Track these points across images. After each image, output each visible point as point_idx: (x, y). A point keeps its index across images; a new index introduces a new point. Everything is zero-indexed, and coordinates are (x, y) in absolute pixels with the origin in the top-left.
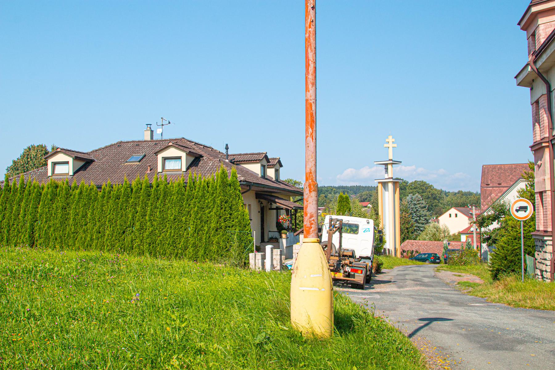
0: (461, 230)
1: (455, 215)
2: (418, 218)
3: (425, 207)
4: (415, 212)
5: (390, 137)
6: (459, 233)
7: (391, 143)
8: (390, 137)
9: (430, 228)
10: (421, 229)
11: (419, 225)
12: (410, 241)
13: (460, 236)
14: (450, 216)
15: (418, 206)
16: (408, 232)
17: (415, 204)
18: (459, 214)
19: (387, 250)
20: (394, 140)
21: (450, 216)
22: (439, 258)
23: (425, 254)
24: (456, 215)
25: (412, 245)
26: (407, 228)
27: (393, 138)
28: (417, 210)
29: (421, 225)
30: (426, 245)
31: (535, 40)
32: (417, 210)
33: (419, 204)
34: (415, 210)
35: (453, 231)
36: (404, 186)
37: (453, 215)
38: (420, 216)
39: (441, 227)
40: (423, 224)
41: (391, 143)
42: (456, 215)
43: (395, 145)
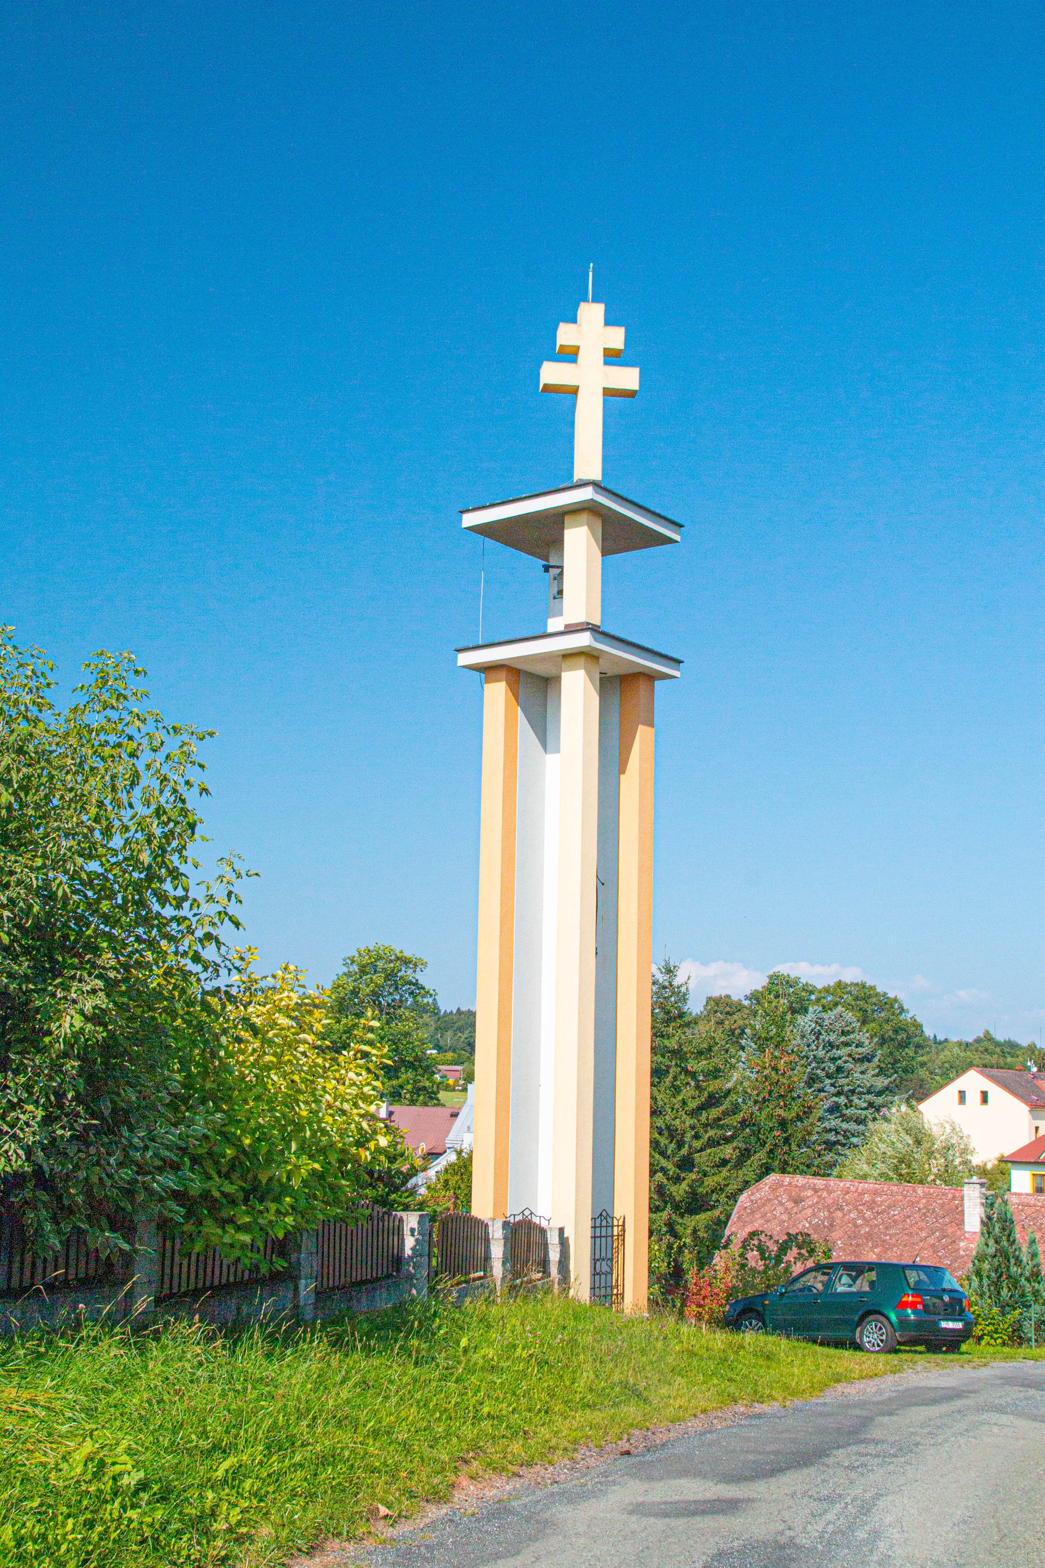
0: (1008, 1151)
1: (978, 1098)
2: (842, 1100)
3: (867, 1059)
4: (829, 1076)
5: (592, 313)
6: (1002, 1160)
7: (591, 356)
8: (592, 313)
9: (886, 1134)
10: (854, 1140)
11: (845, 1125)
12: (787, 1179)
13: (1005, 1174)
14: (962, 1095)
15: (843, 1051)
16: (787, 1141)
17: (831, 1045)
18: (996, 1092)
19: (553, 1239)
20: (616, 338)
21: (962, 1095)
22: (955, 1306)
23: (856, 1269)
24: (984, 1098)
25: (797, 1201)
26: (783, 1124)
27: (609, 321)
28: (839, 1069)
29: (852, 1126)
30: (871, 1205)
31: (666, 1515)
32: (839, 1069)
33: (847, 1044)
34: (833, 1068)
35: (985, 1153)
36: (802, 1000)
37: (973, 1098)
38: (853, 1092)
39: (936, 1131)
40: (859, 1121)
41: (591, 356)
42: (984, 1098)
43: (629, 378)
